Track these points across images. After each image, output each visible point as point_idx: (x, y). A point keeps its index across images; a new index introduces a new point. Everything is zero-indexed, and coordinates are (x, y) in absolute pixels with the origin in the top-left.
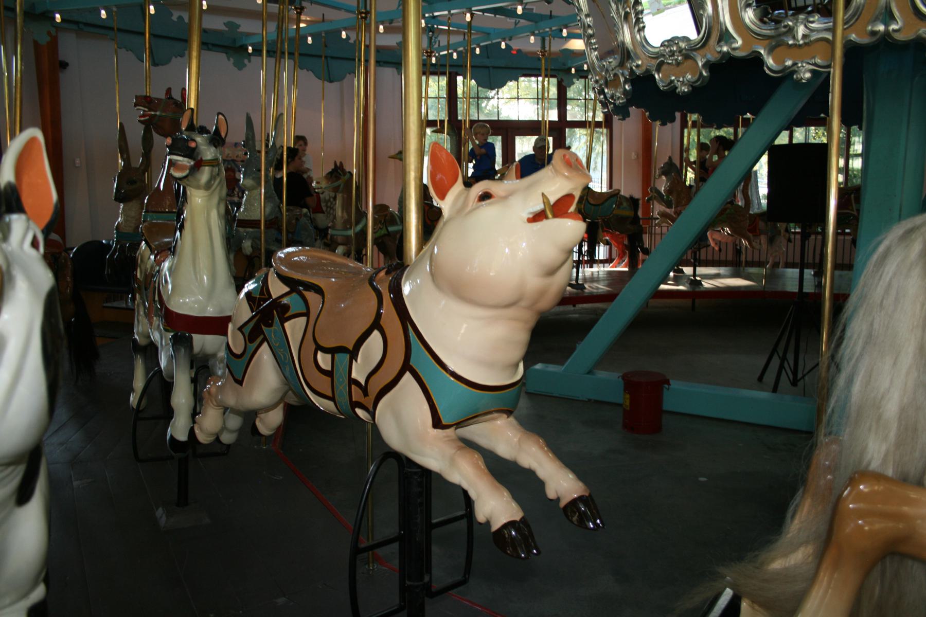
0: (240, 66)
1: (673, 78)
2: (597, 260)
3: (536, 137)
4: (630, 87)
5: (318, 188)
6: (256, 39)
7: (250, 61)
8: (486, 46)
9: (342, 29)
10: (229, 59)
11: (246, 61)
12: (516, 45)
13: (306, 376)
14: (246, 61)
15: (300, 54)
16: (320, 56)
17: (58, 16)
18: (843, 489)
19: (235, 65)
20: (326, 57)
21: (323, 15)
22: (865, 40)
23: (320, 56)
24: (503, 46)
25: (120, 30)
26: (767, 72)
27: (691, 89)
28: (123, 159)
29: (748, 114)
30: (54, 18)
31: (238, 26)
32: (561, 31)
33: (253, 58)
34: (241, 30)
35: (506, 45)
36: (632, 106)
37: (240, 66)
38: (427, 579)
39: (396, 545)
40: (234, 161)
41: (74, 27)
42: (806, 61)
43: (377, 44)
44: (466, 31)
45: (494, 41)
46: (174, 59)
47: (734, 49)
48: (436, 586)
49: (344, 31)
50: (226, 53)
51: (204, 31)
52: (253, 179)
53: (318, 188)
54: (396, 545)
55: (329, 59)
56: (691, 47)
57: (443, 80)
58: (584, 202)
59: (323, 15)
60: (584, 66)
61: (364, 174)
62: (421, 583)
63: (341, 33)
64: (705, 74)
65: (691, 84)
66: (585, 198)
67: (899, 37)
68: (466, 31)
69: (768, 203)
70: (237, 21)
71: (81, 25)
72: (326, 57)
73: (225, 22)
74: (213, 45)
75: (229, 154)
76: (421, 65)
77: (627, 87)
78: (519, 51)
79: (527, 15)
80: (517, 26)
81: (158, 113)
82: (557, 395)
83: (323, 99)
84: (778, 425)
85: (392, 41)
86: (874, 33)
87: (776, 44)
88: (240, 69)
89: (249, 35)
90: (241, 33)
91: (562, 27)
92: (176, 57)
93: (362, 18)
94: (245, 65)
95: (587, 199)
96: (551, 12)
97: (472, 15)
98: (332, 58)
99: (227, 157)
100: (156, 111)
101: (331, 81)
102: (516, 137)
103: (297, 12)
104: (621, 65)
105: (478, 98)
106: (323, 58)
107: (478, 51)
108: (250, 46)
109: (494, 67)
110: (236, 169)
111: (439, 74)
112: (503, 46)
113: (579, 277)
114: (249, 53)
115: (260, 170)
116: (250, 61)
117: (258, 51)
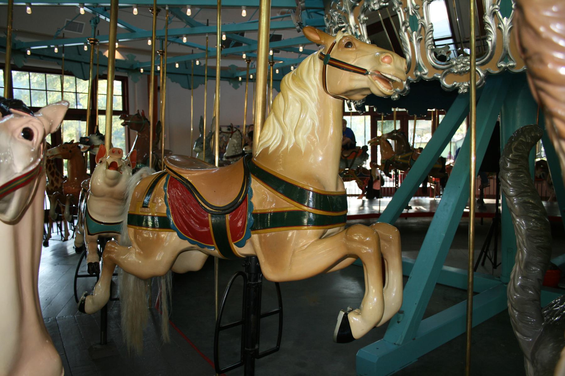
0: (236, 87)
2: (378, 191)
5: (246, 151)
7: (241, 84)
11: (239, 85)
14: (239, 85)
15: (204, 76)
19: (233, 87)
25: (100, 65)
30: (26, 53)
31: (135, 57)
34: (136, 60)
37: (236, 87)
38: (257, 347)
39: (240, 327)
43: (114, 109)
46: (200, 85)
48: (261, 351)
52: (200, 147)
53: (246, 151)
58: (409, 159)
61: (412, 138)
63: (276, 71)
66: (410, 157)
67: (515, 70)
81: (129, 121)
84: (450, 285)
92: (201, 84)
93: (271, 65)
94: (239, 87)
95: (412, 158)
100: (128, 120)
103: (248, 63)
105: (46, 90)
107: (177, 66)
108: (143, 68)
115: (203, 143)
116: (241, 84)
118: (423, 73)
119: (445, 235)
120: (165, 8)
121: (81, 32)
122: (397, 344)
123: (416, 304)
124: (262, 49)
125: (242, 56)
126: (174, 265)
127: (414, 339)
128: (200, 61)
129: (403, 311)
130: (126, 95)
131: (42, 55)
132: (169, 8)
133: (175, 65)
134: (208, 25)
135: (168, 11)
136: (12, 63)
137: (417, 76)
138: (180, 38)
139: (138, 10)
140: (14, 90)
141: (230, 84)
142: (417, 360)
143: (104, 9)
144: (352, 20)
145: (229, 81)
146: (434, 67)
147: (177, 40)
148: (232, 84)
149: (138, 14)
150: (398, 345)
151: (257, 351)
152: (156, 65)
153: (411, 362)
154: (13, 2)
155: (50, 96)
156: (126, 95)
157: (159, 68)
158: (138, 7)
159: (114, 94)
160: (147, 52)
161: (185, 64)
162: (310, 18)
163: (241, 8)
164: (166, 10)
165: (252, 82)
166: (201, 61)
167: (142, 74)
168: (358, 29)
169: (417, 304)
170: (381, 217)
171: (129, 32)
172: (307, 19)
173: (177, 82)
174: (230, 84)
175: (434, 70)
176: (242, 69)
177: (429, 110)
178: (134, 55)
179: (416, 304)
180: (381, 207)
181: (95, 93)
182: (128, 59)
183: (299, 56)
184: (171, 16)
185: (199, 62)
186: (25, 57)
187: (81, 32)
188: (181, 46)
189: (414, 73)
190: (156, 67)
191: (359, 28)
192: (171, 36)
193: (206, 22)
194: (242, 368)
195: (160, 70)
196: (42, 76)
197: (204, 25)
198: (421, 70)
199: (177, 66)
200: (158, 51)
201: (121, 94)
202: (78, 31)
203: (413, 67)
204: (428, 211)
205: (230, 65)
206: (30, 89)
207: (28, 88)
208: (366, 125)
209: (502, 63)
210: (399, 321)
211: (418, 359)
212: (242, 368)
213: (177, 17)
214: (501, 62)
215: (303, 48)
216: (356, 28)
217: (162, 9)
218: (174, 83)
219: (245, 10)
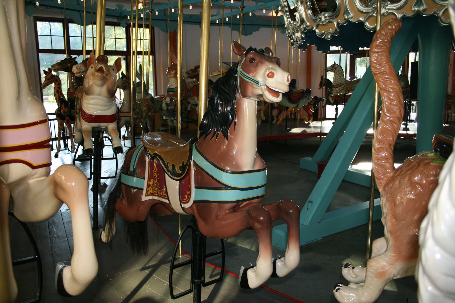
3: (48, 71)
4: (305, 36)
9: (249, 12)
12: (257, 13)
16: (233, 24)
17: (37, 3)
18: (424, 214)
19: (281, 32)
24: (250, 14)
25: (66, 9)
29: (69, 58)
30: (36, 4)
31: (123, 6)
32: (278, 7)
35: (252, 14)
38: (203, 279)
54: (207, 252)
57: (112, 28)
60: (216, 21)
62: (200, 281)
69: (155, 140)
73: (117, 4)
80: (257, 5)
82: (310, 171)
85: (196, 12)
91: (279, 5)
92: (255, 31)
98: (247, 25)
101: (246, 35)
105: (115, 38)
106: (223, 23)
109: (247, 25)
111: (92, 23)
112: (250, 14)
113: (118, 171)
114: (128, 19)
118: (350, 16)
119: (351, 145)
122: (305, 225)
123: (321, 196)
124: (442, 2)
127: (319, 223)
129: (312, 201)
131: (48, 6)
137: (345, 19)
140: (70, 38)
142: (322, 238)
150: (305, 225)
153: (317, 239)
155: (113, 42)
159: (39, 33)
161: (164, 12)
165: (219, 25)
169: (322, 197)
177: (360, 49)
178: (123, 4)
179: (321, 196)
180: (320, 126)
181: (129, 38)
183: (256, 4)
186: (35, 7)
189: (343, 17)
195: (143, 17)
198: (348, 14)
208: (51, 45)
209: (415, 7)
210: (308, 208)
211: (323, 238)
214: (415, 6)
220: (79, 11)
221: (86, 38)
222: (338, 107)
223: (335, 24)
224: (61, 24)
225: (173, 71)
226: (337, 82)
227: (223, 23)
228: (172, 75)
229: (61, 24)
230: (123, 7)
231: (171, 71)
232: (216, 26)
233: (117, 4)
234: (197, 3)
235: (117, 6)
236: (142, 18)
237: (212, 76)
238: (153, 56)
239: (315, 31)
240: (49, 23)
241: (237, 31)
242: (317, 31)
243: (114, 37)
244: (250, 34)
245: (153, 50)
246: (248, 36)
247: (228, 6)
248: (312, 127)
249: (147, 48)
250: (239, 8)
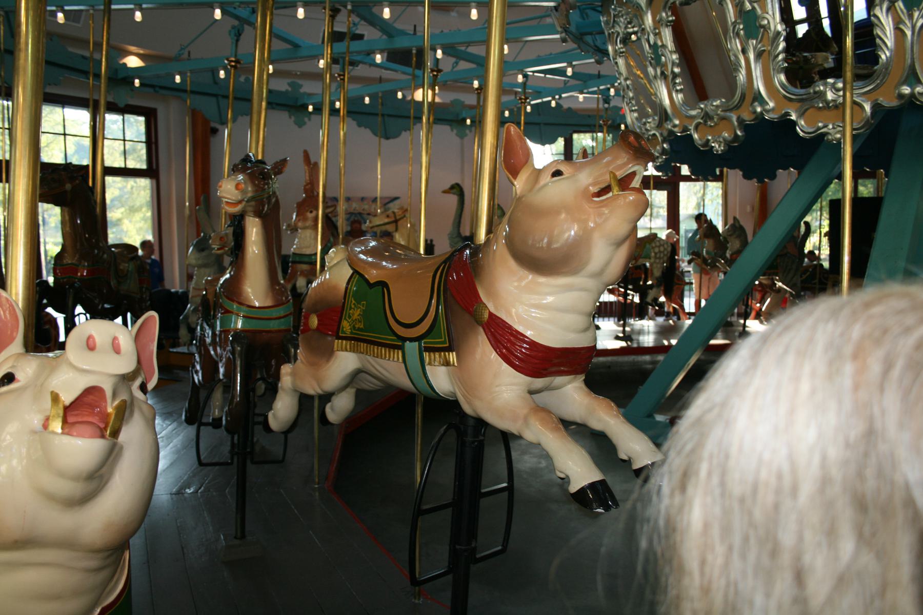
0: (300, 124)
1: (710, 138)
4: (669, 146)
6: (317, 100)
7: (310, 120)
8: (537, 104)
10: (290, 117)
11: (306, 119)
13: (266, 317)
14: (306, 119)
16: (377, 115)
19: (457, 135)
20: (383, 115)
21: (415, 26)
22: (893, 103)
23: (377, 115)
26: (801, 134)
27: (727, 148)
28: (780, 289)
30: (133, 83)
31: (301, 86)
33: (313, 117)
34: (302, 90)
36: (741, 170)
37: (300, 124)
39: (449, 511)
40: (360, 214)
41: (151, 90)
42: (837, 124)
44: (520, 90)
45: (545, 100)
47: (768, 111)
49: (400, 91)
50: (289, 111)
51: (270, 92)
54: (449, 511)
55: (220, 98)
56: (728, 106)
59: (415, 26)
64: (739, 133)
65: (727, 143)
68: (520, 90)
70: (300, 82)
71: (157, 89)
72: (383, 115)
74: (277, 104)
75: (356, 207)
76: (482, 122)
77: (665, 146)
78: (569, 109)
79: (575, 75)
83: (379, 154)
86: (901, 96)
87: (807, 104)
88: (300, 126)
89: (310, 95)
90: (305, 93)
92: (242, 115)
94: (305, 123)
96: (599, 72)
97: (525, 76)
98: (546, 124)
99: (354, 210)
101: (387, 138)
102: (665, 193)
104: (660, 126)
105: (124, 140)
106: (412, 116)
107: (367, 100)
109: (546, 124)
110: (362, 222)
116: (310, 120)
117: (318, 110)
120: (345, 7)
121: (78, 22)
125: (473, 84)
126: (149, 511)
128: (404, 92)
130: (153, 140)
132: (353, 6)
133: (364, 100)
134: (415, 33)
135: (352, 11)
136: (110, 99)
138: (372, 55)
139: (305, 11)
141: (452, 130)
143: (251, 11)
144: (649, 20)
145: (451, 125)
146: (785, 97)
147: (367, 59)
148: (455, 131)
149: (305, 18)
151: (474, 551)
152: (332, 99)
154: (110, 3)
156: (153, 140)
157: (338, 104)
158: (306, 6)
160: (318, 76)
162: (584, 19)
163: (469, 6)
164: (348, 10)
166: (405, 92)
167: (310, 113)
168: (658, 36)
170: (670, 352)
171: (292, 47)
172: (581, 20)
173: (366, 128)
174: (290, 117)
175: (786, 102)
176: (472, 107)
182: (290, 89)
184: (357, 20)
185: (403, 95)
186: (132, 90)
187: (78, 22)
188: (373, 68)
190: (332, 104)
191: (659, 34)
192: (356, 52)
193: (412, 28)
194: (450, 577)
195: (340, 108)
196: (44, 110)
197: (410, 34)
199: (367, 100)
200: (228, 60)
201: (144, 139)
202: (73, 21)
203: (749, 99)
204: (897, 106)
205: (452, 99)
206: (124, 140)
207: (63, 132)
212: (450, 577)
213: (365, 19)
215: (573, 69)
216: (655, 34)
217: (342, 8)
218: (363, 129)
219: (476, 8)
220: (215, 96)
221: (105, 141)
222: (612, 319)
223: (734, 119)
224: (142, 119)
225: (311, 212)
226: (663, 252)
227: (412, 116)
228: (309, 223)
229: (142, 119)
230: (301, 88)
231: (307, 211)
232: (445, 124)
233: (289, 81)
234: (446, 81)
235: (289, 84)
236: (338, 110)
237: (371, 225)
238: (154, 181)
239: (691, 136)
240: (122, 117)
241: (368, 129)
242: (696, 136)
243: (126, 142)
244: (396, 135)
245: (154, 167)
246: (391, 141)
247: (300, 72)
248: (61, 406)
249: (138, 161)
250: (336, 77)
